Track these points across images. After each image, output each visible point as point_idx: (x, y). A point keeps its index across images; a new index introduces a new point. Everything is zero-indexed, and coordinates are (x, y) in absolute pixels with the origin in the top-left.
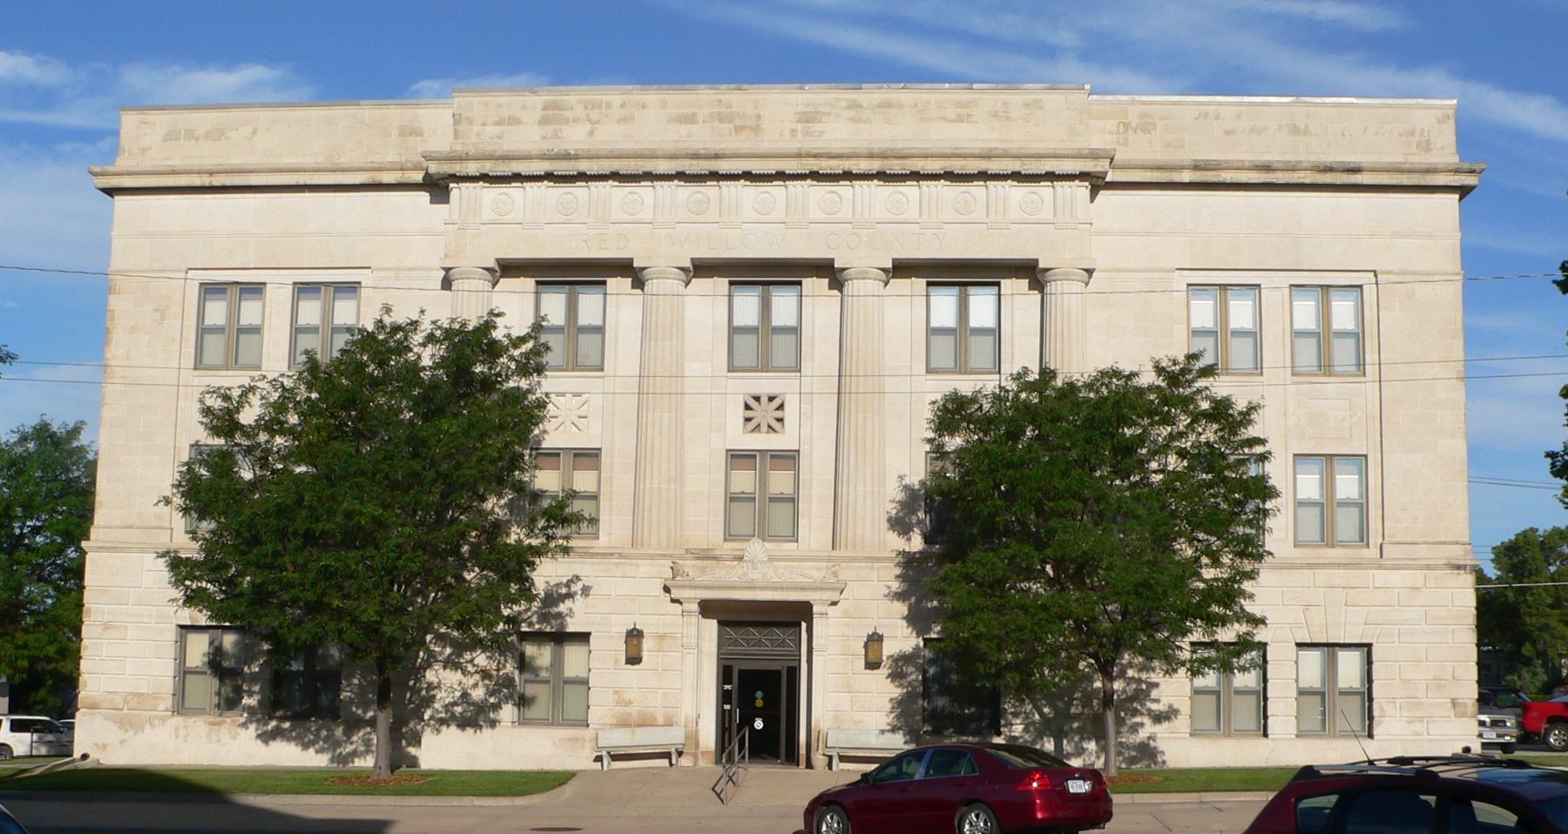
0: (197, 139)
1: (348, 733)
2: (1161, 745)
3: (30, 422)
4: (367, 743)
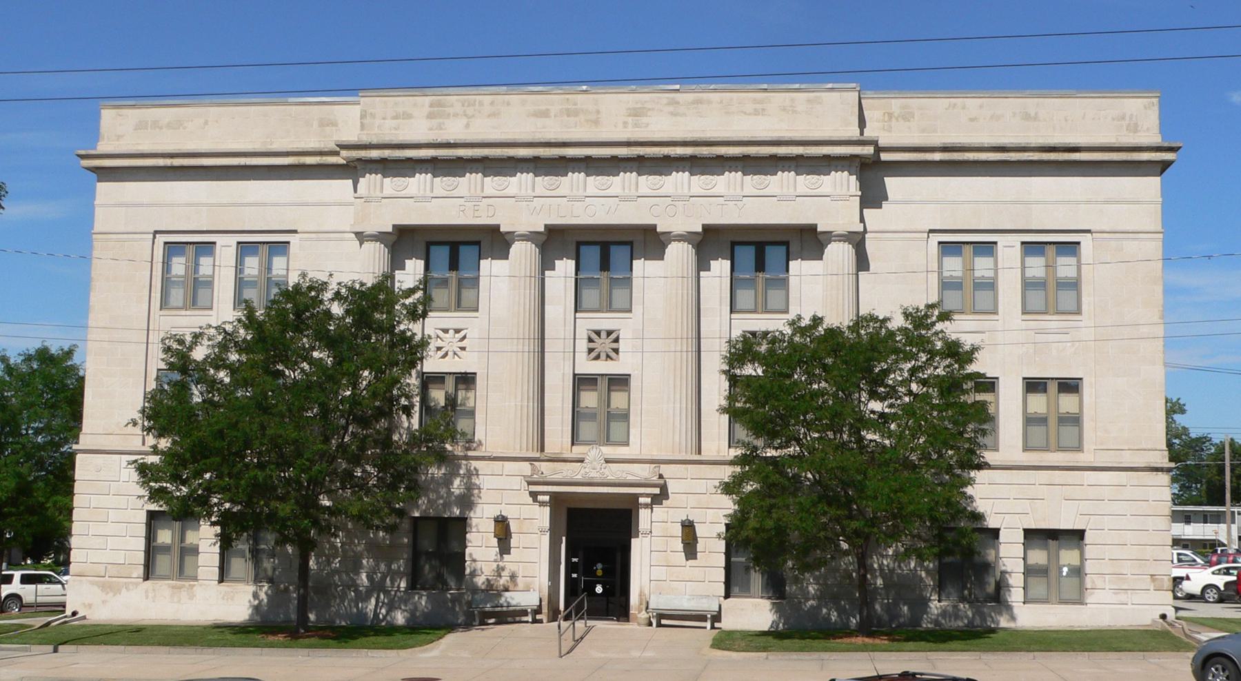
0: (161, 128)
3: (33, 346)
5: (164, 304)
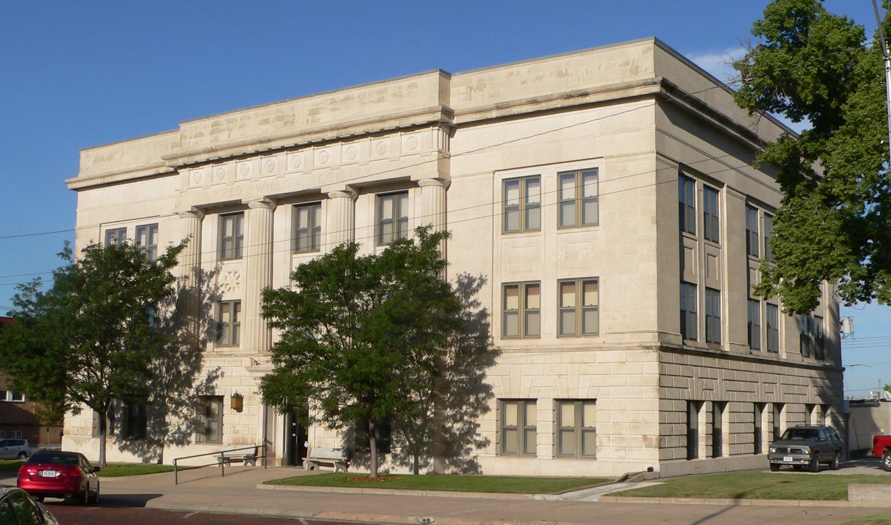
1: (149, 448)
2: (480, 461)
4: (155, 452)
5: (506, 230)
